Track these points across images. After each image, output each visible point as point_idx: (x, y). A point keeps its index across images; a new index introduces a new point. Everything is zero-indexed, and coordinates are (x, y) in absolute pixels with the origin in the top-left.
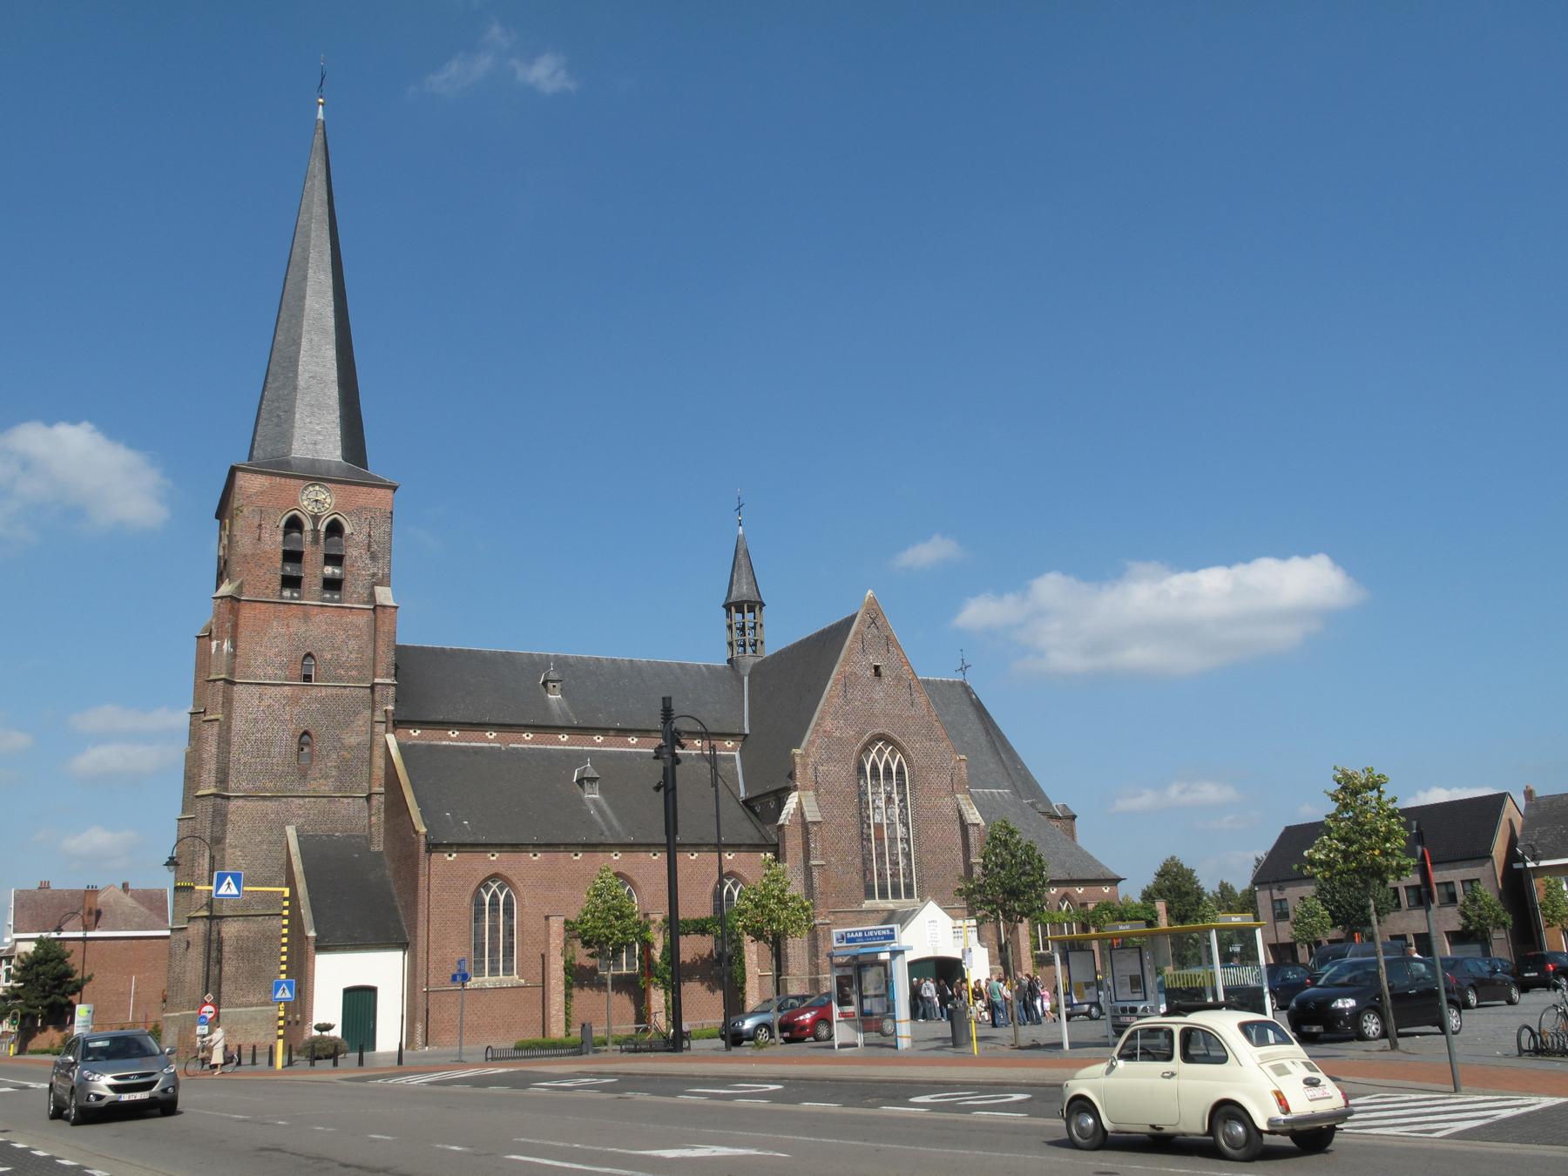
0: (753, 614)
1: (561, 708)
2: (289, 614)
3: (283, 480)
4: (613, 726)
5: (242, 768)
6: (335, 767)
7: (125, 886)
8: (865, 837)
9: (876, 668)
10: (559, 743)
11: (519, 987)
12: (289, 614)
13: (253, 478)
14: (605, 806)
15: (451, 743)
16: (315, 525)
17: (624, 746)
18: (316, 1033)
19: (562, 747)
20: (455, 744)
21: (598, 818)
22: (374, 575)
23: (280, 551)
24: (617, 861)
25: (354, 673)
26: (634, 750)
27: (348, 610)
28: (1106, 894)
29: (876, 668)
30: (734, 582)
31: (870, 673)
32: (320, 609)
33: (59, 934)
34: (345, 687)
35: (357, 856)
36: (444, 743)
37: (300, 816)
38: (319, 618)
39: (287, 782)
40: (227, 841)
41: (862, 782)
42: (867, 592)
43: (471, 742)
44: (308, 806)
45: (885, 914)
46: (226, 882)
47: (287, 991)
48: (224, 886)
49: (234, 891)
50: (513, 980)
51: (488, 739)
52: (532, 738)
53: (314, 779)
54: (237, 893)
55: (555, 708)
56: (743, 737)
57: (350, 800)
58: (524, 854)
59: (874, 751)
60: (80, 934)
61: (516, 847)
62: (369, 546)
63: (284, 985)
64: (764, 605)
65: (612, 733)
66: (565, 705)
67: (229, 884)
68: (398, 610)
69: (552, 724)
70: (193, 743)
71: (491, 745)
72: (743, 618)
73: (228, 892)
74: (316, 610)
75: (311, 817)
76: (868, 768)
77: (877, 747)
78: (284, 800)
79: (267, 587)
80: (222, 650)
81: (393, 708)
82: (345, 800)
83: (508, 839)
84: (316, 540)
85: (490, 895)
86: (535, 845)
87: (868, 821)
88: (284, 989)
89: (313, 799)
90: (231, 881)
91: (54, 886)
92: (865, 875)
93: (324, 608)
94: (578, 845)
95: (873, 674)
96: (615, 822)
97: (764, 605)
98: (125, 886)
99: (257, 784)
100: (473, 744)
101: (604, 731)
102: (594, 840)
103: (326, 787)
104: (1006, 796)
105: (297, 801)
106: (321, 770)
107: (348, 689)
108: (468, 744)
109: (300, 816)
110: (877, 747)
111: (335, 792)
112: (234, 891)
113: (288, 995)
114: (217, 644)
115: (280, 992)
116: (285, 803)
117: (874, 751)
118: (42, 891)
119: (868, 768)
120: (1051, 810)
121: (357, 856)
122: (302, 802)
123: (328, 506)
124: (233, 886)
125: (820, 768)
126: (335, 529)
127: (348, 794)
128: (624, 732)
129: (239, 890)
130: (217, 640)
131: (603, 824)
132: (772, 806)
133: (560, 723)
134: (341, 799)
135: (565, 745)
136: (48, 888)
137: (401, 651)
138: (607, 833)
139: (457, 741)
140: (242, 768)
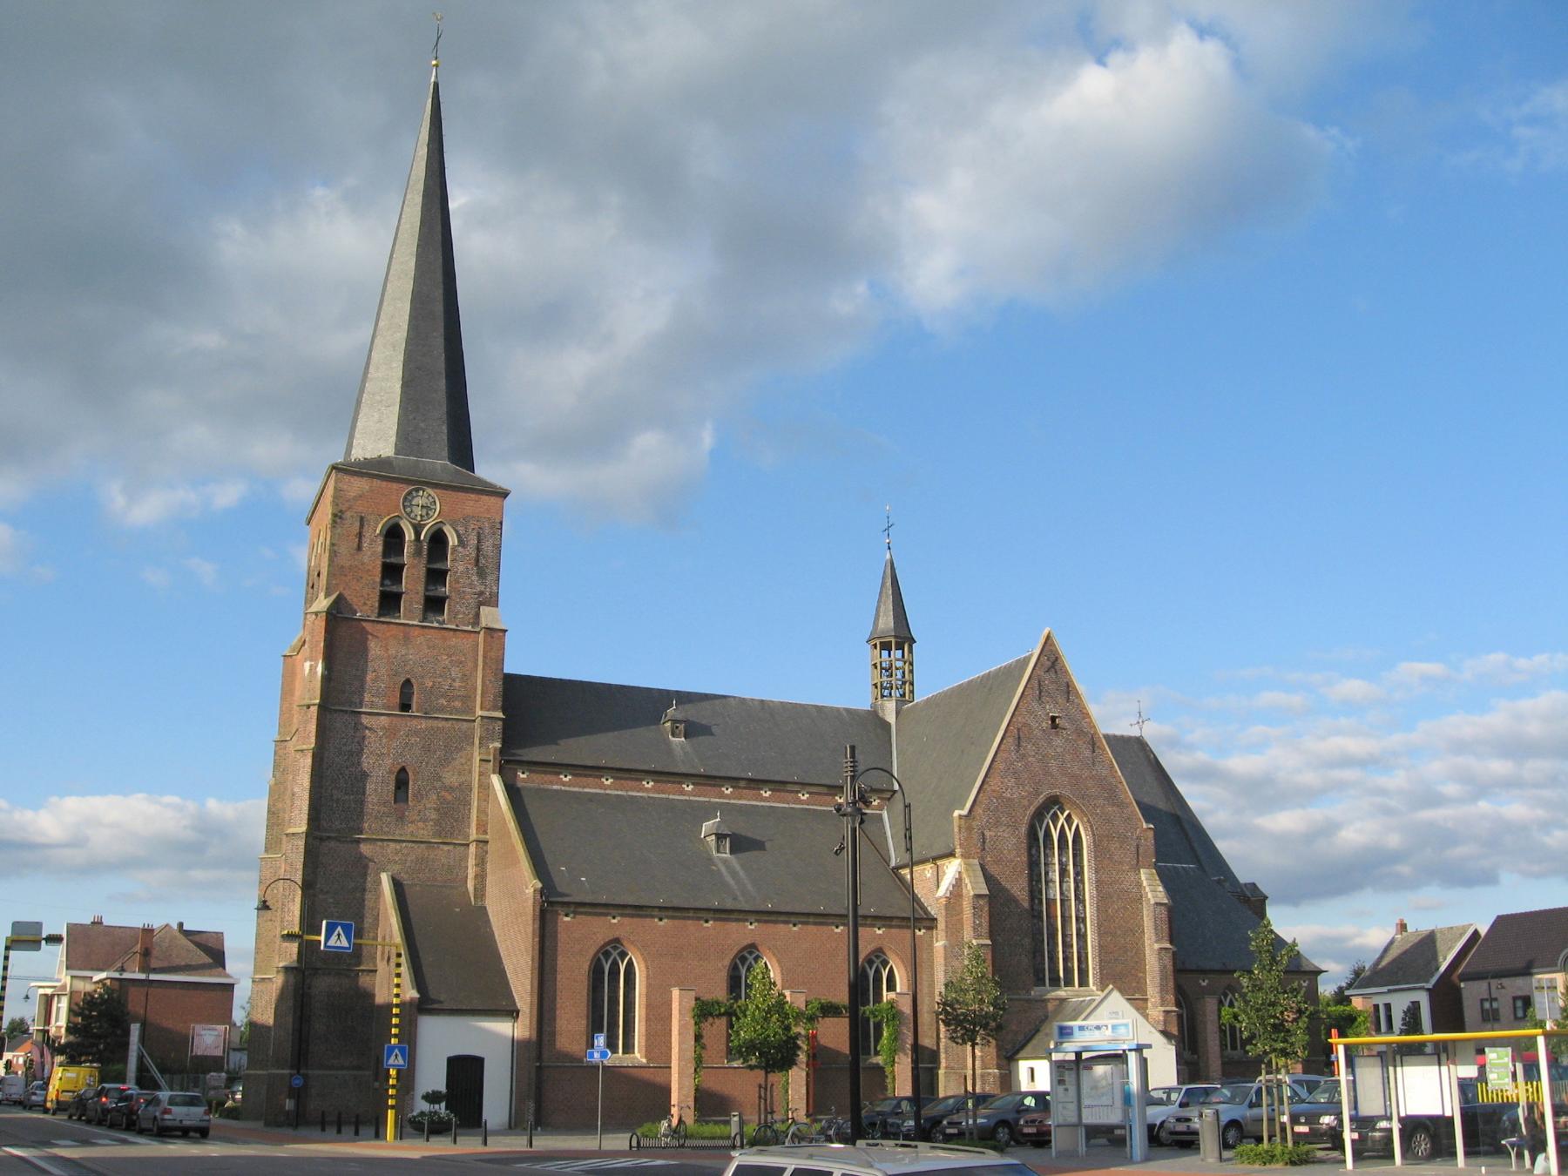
0: (901, 651)
1: (685, 753)
2: (388, 634)
3: (385, 483)
4: (743, 775)
5: (335, 805)
6: (435, 809)
7: (181, 925)
8: (1036, 914)
9: (1053, 719)
10: (683, 792)
11: (641, 1067)
12: (388, 634)
13: (352, 480)
14: (738, 868)
15: (563, 788)
16: (418, 534)
17: (756, 800)
18: (425, 1106)
19: (687, 798)
20: (567, 789)
21: (732, 882)
22: (481, 593)
23: (379, 563)
24: (752, 930)
25: (457, 704)
26: (768, 804)
27: (452, 633)
28: (1204, 987)
29: (1053, 719)
30: (881, 614)
31: (1047, 724)
32: (421, 631)
33: (121, 975)
34: (447, 719)
35: (457, 910)
36: (555, 787)
37: (396, 862)
38: (420, 639)
39: (383, 823)
40: (318, 886)
41: (1034, 851)
42: (1044, 630)
43: (584, 787)
44: (405, 851)
45: (190, 938)
46: (336, 933)
47: (400, 1058)
48: (334, 937)
49: (345, 943)
50: (634, 1058)
51: (605, 785)
52: (612, 783)
53: (412, 822)
54: (346, 945)
55: (678, 751)
56: (891, 793)
57: (451, 847)
58: (648, 920)
59: (1049, 816)
60: (142, 976)
61: (639, 910)
62: (477, 561)
63: (397, 1051)
64: (915, 642)
65: (742, 784)
66: (688, 749)
67: (339, 935)
68: (507, 633)
69: (676, 770)
70: (278, 774)
71: (608, 792)
72: (890, 656)
73: (338, 944)
74: (417, 632)
75: (408, 864)
76: (1041, 835)
77: (1052, 812)
78: (379, 843)
79: (365, 604)
80: (316, 673)
81: (500, 746)
82: (446, 848)
83: (631, 900)
84: (418, 552)
85: (609, 962)
86: (660, 908)
87: (1039, 896)
88: (396, 1055)
89: (410, 845)
90: (341, 932)
91: (105, 923)
92: (1034, 957)
93: (426, 630)
94: (708, 910)
95: (1050, 726)
96: (749, 887)
97: (915, 642)
98: (181, 925)
99: (352, 824)
100: (586, 790)
101: (733, 781)
102: (729, 905)
103: (425, 832)
104: (1192, 873)
105: (392, 845)
106: (419, 812)
107: (450, 722)
108: (581, 790)
109: (396, 862)
110: (1052, 812)
111: (434, 836)
112: (345, 943)
113: (400, 1061)
114: (311, 666)
115: (393, 1057)
116: (381, 847)
117: (1049, 816)
118: (96, 927)
119: (1041, 835)
120: (1239, 890)
121: (457, 910)
122: (398, 847)
123: (406, 504)
124: (343, 938)
125: (987, 833)
126: (438, 539)
127: (449, 841)
128: (756, 783)
129: (349, 942)
130: (311, 661)
131: (736, 887)
132: (929, 875)
133: (683, 770)
134: (441, 846)
135: (689, 795)
136: (101, 923)
137: (512, 682)
138: (741, 898)
139: (569, 786)
140: (335, 805)
